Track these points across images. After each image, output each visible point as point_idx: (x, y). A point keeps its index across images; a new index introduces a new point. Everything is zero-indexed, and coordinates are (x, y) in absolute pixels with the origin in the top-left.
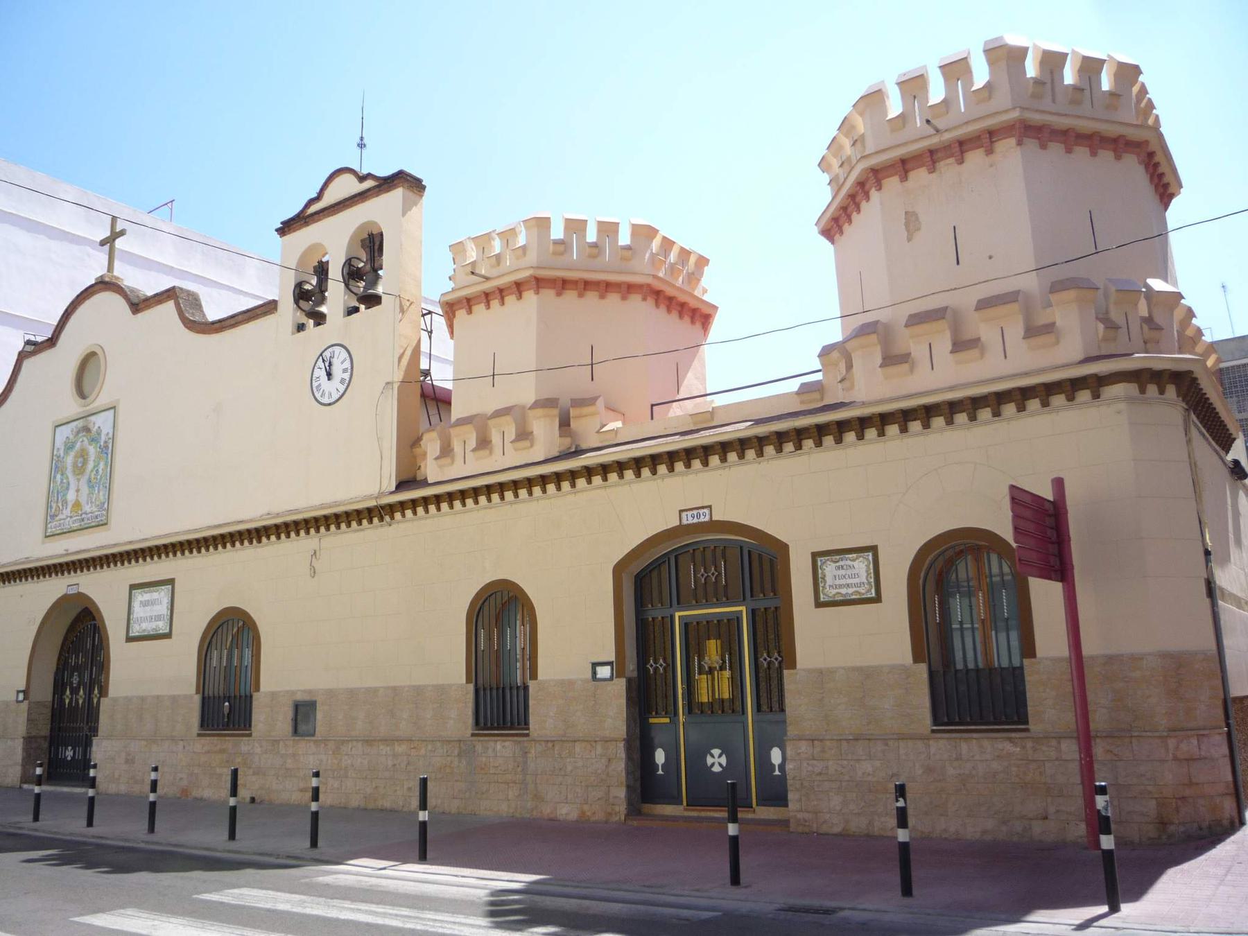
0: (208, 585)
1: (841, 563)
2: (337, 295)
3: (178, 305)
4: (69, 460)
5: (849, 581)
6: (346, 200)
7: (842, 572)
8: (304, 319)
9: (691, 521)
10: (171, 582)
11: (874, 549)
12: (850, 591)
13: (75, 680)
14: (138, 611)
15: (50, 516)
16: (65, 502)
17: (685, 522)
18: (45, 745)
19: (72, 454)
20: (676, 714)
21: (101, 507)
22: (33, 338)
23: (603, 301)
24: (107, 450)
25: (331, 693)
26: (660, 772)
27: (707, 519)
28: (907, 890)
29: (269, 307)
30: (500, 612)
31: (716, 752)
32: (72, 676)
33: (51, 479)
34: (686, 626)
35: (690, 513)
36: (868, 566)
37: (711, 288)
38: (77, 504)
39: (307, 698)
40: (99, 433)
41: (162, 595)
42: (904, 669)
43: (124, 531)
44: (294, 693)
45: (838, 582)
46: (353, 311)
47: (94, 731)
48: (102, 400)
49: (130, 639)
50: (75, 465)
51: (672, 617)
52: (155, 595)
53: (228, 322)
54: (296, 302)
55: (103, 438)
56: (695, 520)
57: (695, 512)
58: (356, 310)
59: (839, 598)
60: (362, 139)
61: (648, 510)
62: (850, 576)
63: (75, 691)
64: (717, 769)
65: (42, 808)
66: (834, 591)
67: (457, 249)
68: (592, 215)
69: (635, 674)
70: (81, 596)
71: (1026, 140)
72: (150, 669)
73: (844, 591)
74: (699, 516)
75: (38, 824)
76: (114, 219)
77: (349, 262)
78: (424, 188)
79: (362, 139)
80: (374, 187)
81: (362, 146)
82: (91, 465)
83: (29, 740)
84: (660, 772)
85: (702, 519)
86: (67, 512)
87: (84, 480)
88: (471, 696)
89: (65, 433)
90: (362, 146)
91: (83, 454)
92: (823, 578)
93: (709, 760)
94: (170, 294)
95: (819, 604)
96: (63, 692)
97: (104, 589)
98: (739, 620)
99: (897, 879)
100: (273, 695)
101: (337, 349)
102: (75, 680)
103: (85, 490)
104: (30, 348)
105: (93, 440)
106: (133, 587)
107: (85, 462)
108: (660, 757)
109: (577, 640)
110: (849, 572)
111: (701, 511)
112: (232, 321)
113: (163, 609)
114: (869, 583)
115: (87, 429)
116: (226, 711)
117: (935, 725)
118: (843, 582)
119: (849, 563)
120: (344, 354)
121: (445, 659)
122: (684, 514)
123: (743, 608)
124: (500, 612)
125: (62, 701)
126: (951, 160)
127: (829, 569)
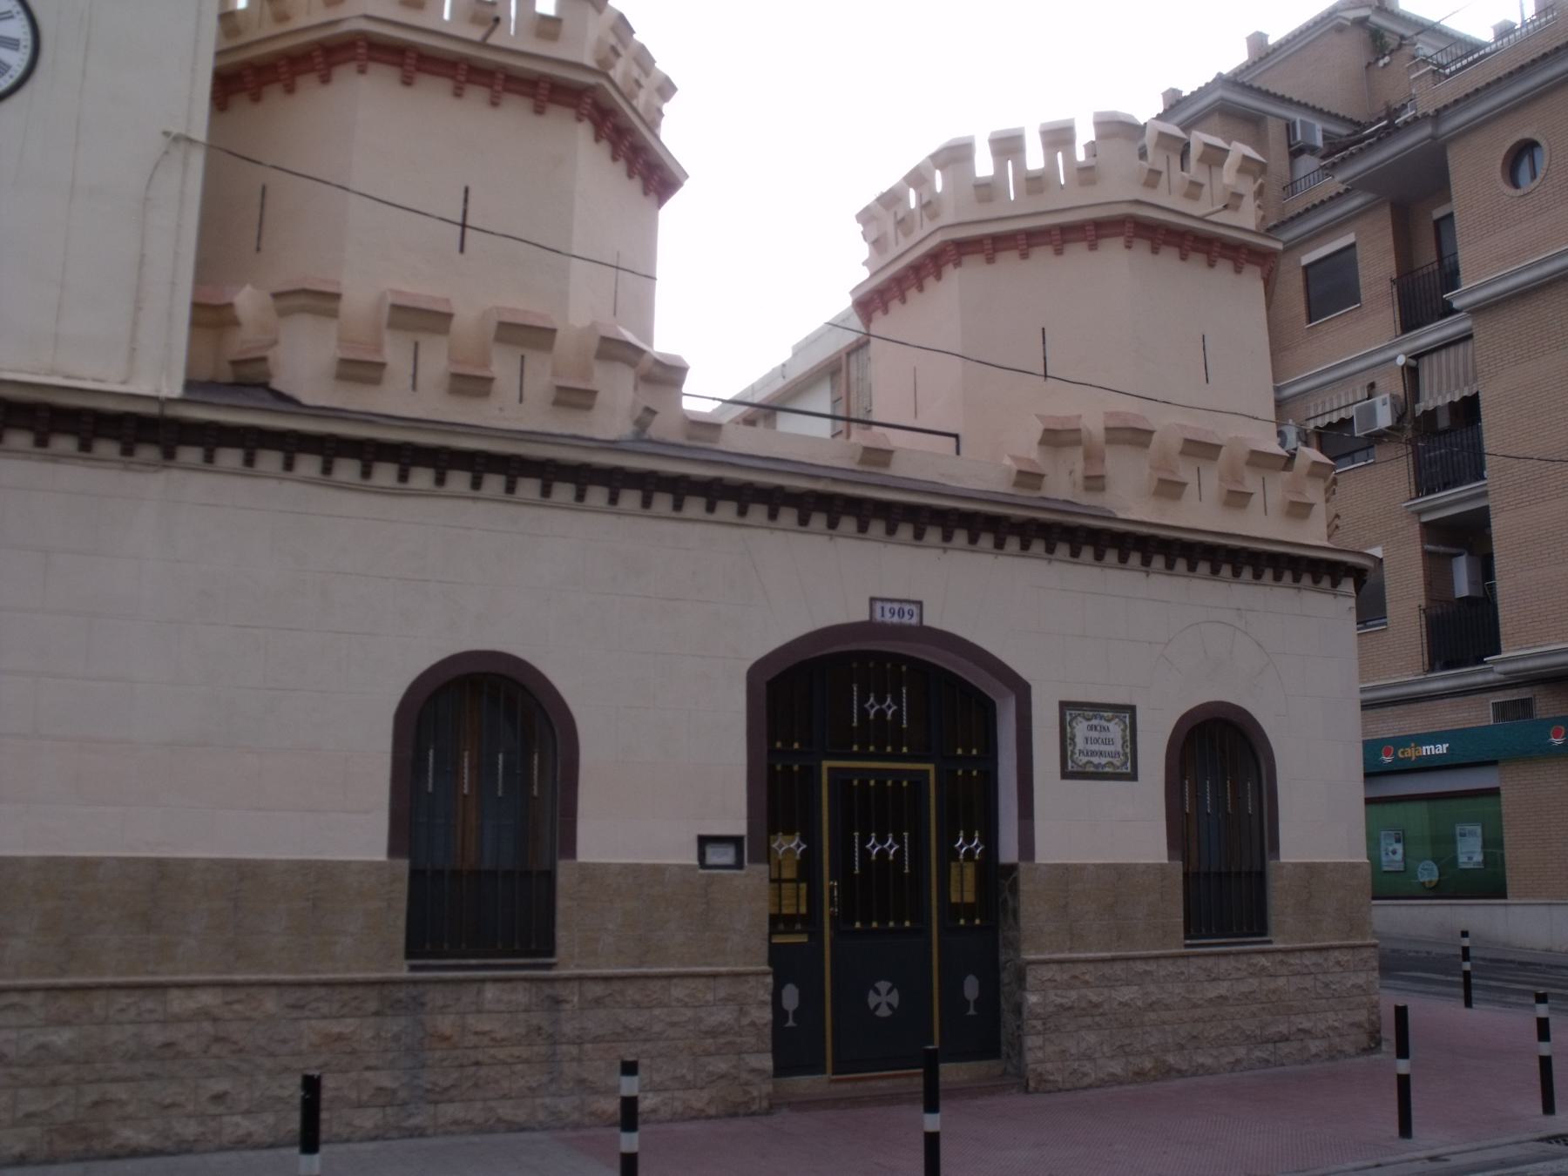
1: (1094, 722)
7: (1095, 734)
9: (888, 618)
12: (1104, 760)
17: (878, 617)
26: (972, 1012)
27: (914, 621)
35: (888, 606)
36: (1124, 731)
37: (677, 133)
51: (811, 773)
56: (896, 619)
57: (896, 606)
59: (1091, 769)
61: (825, 586)
66: (1084, 759)
68: (980, 129)
73: (1096, 760)
74: (901, 613)
84: (972, 1012)
85: (906, 620)
88: (402, 888)
92: (1073, 739)
95: (1066, 775)
110: (1103, 735)
111: (907, 607)
114: (1125, 754)
117: (1186, 938)
118: (1095, 747)
119: (1104, 723)
121: (346, 819)
122: (878, 605)
123: (930, 767)
127: (1081, 729)
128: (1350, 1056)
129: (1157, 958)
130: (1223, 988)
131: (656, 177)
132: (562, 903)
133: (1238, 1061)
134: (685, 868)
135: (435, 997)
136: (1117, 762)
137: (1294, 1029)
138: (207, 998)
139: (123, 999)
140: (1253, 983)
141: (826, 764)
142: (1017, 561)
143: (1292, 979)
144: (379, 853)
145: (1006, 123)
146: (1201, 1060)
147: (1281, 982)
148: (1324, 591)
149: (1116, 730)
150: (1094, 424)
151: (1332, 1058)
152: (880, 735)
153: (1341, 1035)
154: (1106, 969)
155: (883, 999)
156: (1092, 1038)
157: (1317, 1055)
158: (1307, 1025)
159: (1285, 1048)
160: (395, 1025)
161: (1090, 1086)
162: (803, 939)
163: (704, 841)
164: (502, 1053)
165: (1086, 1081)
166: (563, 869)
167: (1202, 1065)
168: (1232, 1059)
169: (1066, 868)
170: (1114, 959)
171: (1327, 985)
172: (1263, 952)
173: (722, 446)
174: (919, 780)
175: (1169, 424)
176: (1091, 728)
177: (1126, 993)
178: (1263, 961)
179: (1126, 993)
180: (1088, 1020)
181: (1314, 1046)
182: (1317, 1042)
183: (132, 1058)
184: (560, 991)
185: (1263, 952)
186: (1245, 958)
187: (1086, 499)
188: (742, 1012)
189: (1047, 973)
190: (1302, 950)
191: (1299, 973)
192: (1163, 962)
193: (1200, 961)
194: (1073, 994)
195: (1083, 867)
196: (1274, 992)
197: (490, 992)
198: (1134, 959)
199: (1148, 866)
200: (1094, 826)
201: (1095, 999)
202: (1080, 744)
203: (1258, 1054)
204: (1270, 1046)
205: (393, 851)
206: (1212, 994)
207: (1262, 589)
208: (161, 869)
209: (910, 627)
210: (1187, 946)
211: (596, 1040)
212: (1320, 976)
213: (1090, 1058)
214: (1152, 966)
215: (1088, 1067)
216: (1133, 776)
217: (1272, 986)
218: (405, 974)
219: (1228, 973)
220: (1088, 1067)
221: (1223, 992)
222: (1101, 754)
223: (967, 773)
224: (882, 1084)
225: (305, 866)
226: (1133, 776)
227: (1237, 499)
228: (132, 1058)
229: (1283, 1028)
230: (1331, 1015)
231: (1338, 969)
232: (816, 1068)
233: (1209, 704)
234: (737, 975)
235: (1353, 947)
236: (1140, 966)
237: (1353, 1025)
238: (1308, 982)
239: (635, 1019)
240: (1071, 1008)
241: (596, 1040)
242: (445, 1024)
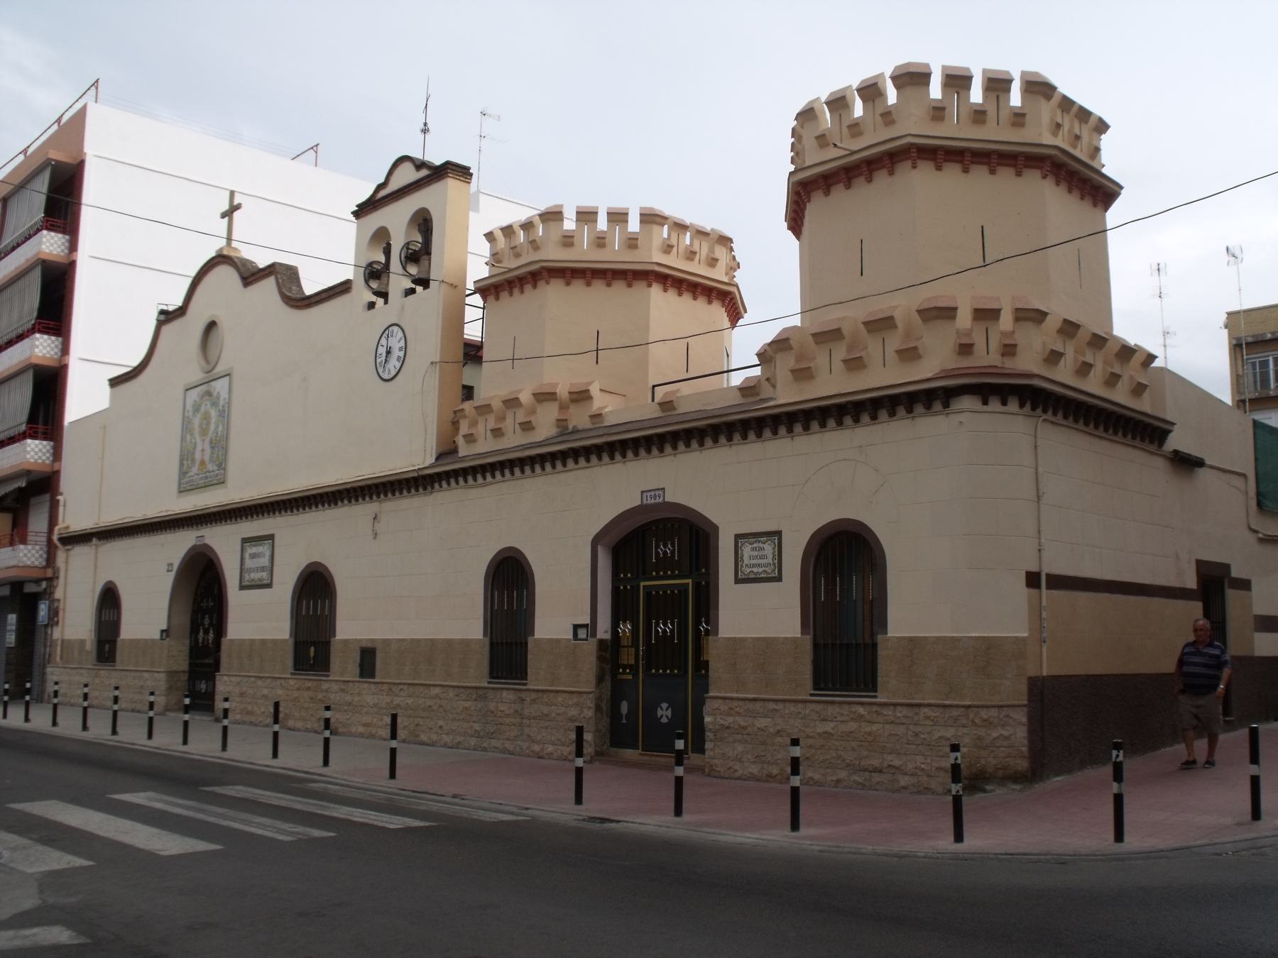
0: (299, 543)
2: (398, 282)
4: (196, 422)
7: (755, 553)
8: (374, 298)
10: (271, 537)
11: (778, 534)
12: (760, 570)
13: (207, 621)
14: (249, 563)
15: (183, 473)
16: (193, 460)
18: (185, 677)
19: (199, 416)
20: (637, 672)
24: (225, 414)
25: (386, 642)
28: (678, 811)
29: (343, 288)
30: (510, 577)
31: (665, 705)
32: (203, 618)
33: (183, 439)
34: (648, 595)
37: (1114, 159)
38: (203, 463)
39: (369, 645)
41: (264, 549)
42: (795, 640)
43: (234, 493)
44: (360, 640)
46: (411, 292)
47: (216, 666)
48: (221, 368)
49: (242, 588)
50: (201, 426)
52: (260, 549)
53: (313, 300)
54: (367, 282)
55: (222, 402)
58: (412, 291)
59: (752, 576)
60: (425, 124)
61: (616, 490)
63: (206, 632)
64: (664, 720)
65: (119, 723)
67: (490, 236)
70: (206, 546)
71: (919, 162)
72: (258, 617)
73: (755, 570)
75: (225, 755)
76: (232, 193)
78: (471, 175)
79: (425, 124)
80: (428, 176)
81: (425, 131)
82: (212, 427)
83: (171, 674)
86: (195, 470)
89: (194, 395)
90: (425, 131)
91: (207, 417)
93: (660, 712)
94: (272, 269)
95: (738, 581)
97: (225, 541)
98: (686, 590)
100: (346, 642)
101: (395, 329)
102: (207, 621)
103: (207, 447)
105: (214, 404)
106: (245, 541)
107: (208, 424)
108: (624, 708)
109: (567, 601)
110: (761, 553)
112: (318, 298)
113: (265, 561)
115: (209, 394)
120: (400, 334)
123: (689, 581)
124: (510, 577)
125: (197, 640)
127: (747, 551)
130: (829, 727)
131: (1102, 193)
132: (529, 656)
133: (838, 781)
135: (491, 694)
137: (885, 764)
138: (437, 690)
140: (853, 726)
141: (642, 584)
143: (887, 726)
144: (481, 637)
145: (587, 203)
148: (937, 413)
149: (769, 549)
152: (665, 565)
153: (929, 776)
154: (750, 706)
155: (664, 713)
156: (740, 748)
157: (905, 788)
158: (897, 763)
159: (877, 778)
160: (480, 705)
163: (576, 627)
164: (507, 720)
165: (737, 775)
166: (530, 639)
168: (834, 778)
169: (735, 639)
170: (755, 700)
171: (917, 734)
176: (753, 549)
177: (762, 722)
178: (861, 710)
179: (762, 722)
180: (739, 737)
181: (904, 781)
182: (906, 778)
184: (524, 695)
188: (582, 712)
189: (716, 704)
194: (730, 719)
196: (870, 734)
197: (505, 694)
198: (769, 700)
199: (786, 639)
201: (743, 724)
202: (746, 561)
203: (856, 778)
204: (867, 774)
205: (485, 634)
208: (433, 642)
209: (658, 504)
210: (812, 695)
211: (534, 718)
212: (911, 727)
213: (740, 761)
214: (779, 706)
215: (737, 766)
216: (779, 579)
217: (868, 729)
218: (486, 685)
219: (840, 718)
220: (737, 766)
223: (625, 587)
224: (663, 760)
226: (779, 579)
227: (854, 364)
228: (424, 710)
229: (876, 762)
230: (920, 759)
231: (928, 722)
232: (635, 747)
233: (184, 559)
234: (580, 693)
235: (944, 706)
236: (772, 706)
237: (938, 769)
238: (901, 730)
239: (545, 710)
240: (728, 728)
241: (534, 718)
242: (492, 706)
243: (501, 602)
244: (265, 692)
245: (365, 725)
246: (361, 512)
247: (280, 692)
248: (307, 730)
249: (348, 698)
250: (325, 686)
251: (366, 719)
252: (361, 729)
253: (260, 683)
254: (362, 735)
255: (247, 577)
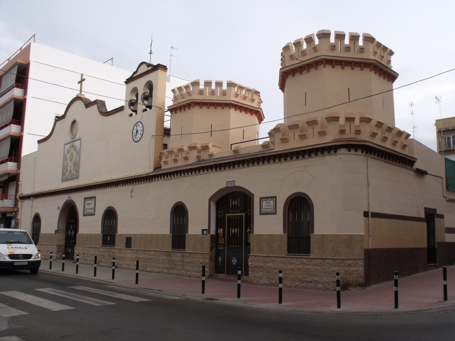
0: (105, 199)
2: (141, 107)
3: (98, 106)
4: (68, 156)
5: (269, 207)
6: (143, 73)
7: (267, 204)
8: (132, 112)
11: (275, 197)
12: (269, 210)
13: (71, 227)
14: (87, 207)
15: (63, 174)
16: (67, 170)
19: (69, 154)
20: (225, 246)
21: (76, 172)
22: (58, 115)
23: (216, 110)
24: (79, 153)
25: (136, 235)
28: (239, 296)
30: (179, 212)
31: (234, 258)
32: (70, 226)
33: (64, 162)
34: (229, 219)
38: (70, 171)
40: (76, 147)
41: (92, 202)
42: (281, 235)
43: (82, 181)
45: (266, 207)
46: (145, 110)
48: (77, 137)
49: (84, 215)
50: (70, 158)
52: (91, 202)
54: (129, 107)
55: (77, 149)
58: (146, 110)
59: (266, 212)
60: (151, 51)
61: (217, 181)
62: (268, 205)
63: (71, 231)
64: (234, 264)
67: (173, 91)
69: (214, 234)
73: (267, 210)
76: (82, 75)
77: (144, 94)
79: (151, 51)
81: (151, 53)
82: (74, 158)
83: (58, 246)
86: (68, 173)
87: (72, 163)
88: (171, 238)
89: (68, 147)
90: (151, 53)
91: (72, 154)
93: (233, 261)
94: (96, 102)
96: (68, 231)
97: (78, 199)
98: (242, 218)
99: (236, 294)
100: (121, 235)
101: (140, 123)
102: (71, 227)
104: (57, 119)
105: (75, 150)
106: (85, 199)
108: (220, 259)
109: (200, 221)
110: (269, 204)
112: (112, 112)
113: (92, 206)
115: (73, 146)
116: (109, 239)
118: (267, 207)
120: (141, 125)
121: (164, 228)
123: (243, 214)
124: (179, 212)
126: (306, 71)
127: (264, 203)
128: (332, 291)
129: (277, 257)
130: (293, 266)
133: (296, 286)
134: (200, 235)
135: (172, 254)
136: (272, 210)
139: (148, 252)
140: (302, 266)
141: (227, 215)
142: (309, 160)
143: (314, 266)
146: (286, 283)
147: (309, 267)
149: (272, 203)
150: (199, 146)
151: (325, 290)
152: (235, 208)
154: (265, 259)
156: (261, 274)
157: (320, 288)
158: (317, 279)
159: (310, 285)
160: (168, 258)
161: (261, 285)
162: (222, 248)
163: (203, 230)
165: (260, 283)
167: (286, 285)
170: (267, 257)
171: (324, 269)
172: (305, 258)
173: (241, 153)
174: (241, 217)
175: (320, 116)
176: (266, 203)
177: (269, 265)
178: (304, 260)
179: (269, 265)
180: (261, 270)
181: (320, 286)
182: (321, 285)
183: (148, 259)
184: (184, 254)
185: (305, 258)
186: (299, 259)
187: (342, 137)
190: (317, 259)
191: (316, 265)
192: (278, 258)
193: (287, 259)
194: (258, 264)
195: (263, 235)
196: (307, 269)
198: (271, 257)
199: (278, 235)
200: (268, 225)
201: (262, 265)
204: (306, 284)
206: (290, 268)
207: (312, 159)
211: (188, 263)
213: (261, 278)
214: (275, 259)
216: (275, 213)
217: (307, 267)
218: (171, 251)
219: (297, 263)
221: (293, 267)
222: (268, 209)
224: (234, 278)
225: (162, 235)
226: (275, 213)
227: (303, 137)
230: (325, 278)
232: (224, 273)
234: (204, 254)
236: (272, 259)
237: (332, 282)
238: (319, 268)
239: (192, 260)
240: (257, 266)
241: (188, 263)
242: (173, 258)
243: (110, 223)
244: (92, 253)
245: (128, 265)
246: (127, 188)
247: (97, 253)
248: (107, 266)
249: (122, 255)
250: (113, 251)
251: (128, 263)
252: (126, 266)
253: (90, 249)
254: (126, 268)
255: (86, 211)
